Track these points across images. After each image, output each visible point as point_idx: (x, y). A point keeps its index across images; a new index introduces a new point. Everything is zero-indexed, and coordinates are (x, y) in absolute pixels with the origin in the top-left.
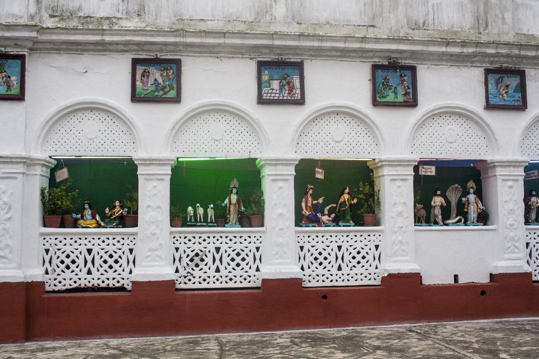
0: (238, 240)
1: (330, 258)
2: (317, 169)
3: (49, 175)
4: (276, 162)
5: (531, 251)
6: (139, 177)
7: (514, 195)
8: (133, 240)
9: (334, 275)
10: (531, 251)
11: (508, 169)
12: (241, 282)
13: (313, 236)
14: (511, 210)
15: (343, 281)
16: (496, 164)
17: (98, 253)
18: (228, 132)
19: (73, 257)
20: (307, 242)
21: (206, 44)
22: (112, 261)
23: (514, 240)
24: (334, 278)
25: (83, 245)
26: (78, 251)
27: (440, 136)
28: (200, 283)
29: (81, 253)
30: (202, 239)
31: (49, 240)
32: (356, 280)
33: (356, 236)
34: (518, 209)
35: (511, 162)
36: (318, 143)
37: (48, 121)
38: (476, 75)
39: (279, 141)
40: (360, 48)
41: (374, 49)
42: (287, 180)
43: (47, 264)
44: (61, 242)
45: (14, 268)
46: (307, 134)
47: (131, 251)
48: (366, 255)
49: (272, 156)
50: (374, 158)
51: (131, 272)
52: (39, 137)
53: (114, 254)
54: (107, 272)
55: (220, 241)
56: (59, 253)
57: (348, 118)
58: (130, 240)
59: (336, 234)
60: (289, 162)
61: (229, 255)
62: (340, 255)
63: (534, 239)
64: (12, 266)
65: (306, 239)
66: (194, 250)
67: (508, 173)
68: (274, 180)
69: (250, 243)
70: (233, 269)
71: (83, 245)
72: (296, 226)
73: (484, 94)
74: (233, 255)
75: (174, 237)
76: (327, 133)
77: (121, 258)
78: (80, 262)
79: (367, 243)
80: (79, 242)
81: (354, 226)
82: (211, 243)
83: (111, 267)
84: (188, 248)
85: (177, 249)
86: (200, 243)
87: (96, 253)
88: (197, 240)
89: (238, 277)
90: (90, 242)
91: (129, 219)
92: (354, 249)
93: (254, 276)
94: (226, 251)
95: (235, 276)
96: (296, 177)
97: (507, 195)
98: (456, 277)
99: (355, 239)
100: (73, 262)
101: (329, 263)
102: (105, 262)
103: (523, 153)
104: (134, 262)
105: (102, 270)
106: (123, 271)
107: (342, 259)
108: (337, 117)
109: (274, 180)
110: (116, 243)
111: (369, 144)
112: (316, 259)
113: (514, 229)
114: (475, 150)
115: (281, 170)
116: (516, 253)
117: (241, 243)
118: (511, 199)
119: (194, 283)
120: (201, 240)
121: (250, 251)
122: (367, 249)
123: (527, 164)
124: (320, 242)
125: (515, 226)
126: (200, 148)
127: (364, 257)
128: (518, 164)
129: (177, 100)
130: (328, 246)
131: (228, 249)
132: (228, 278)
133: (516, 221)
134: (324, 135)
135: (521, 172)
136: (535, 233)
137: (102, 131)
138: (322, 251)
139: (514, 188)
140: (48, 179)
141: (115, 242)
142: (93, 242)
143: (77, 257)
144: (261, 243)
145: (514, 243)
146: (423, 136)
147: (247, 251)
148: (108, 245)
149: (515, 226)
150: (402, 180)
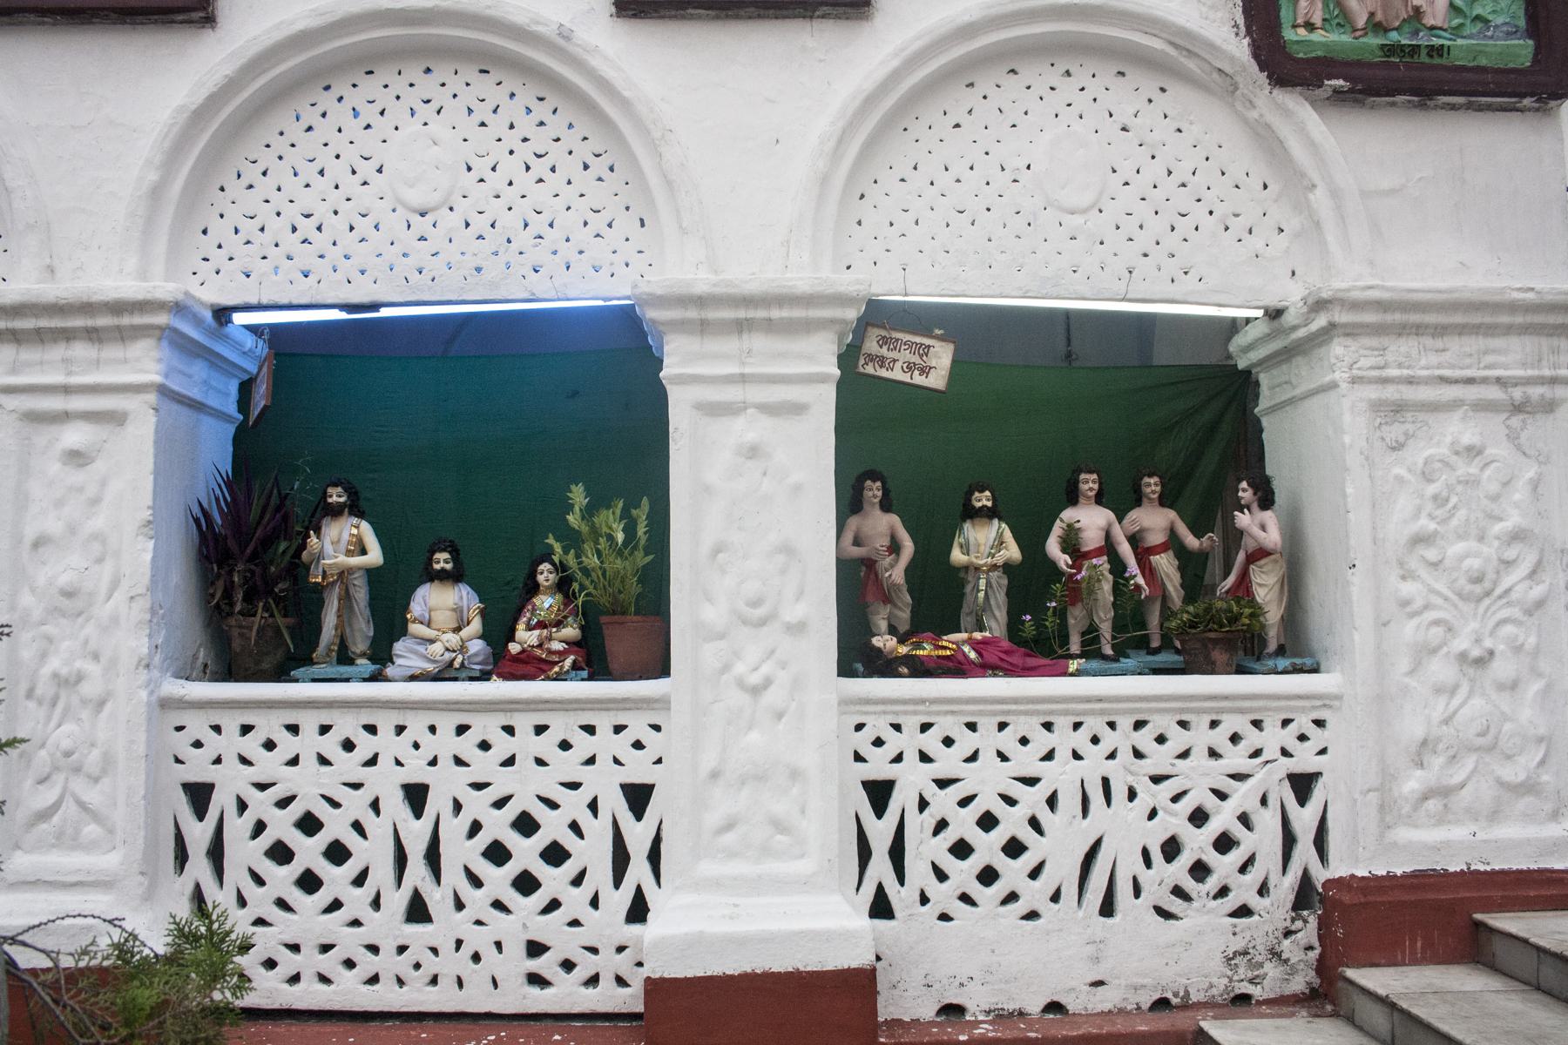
7: (95, 501)
8: (648, 737)
11: (57, 352)
12: (324, 979)
13: (486, 726)
14: (69, 594)
15: (434, 981)
18: (482, 166)
19: (553, 828)
20: (911, 757)
23: (77, 770)
29: (593, 806)
30: (472, 737)
31: (426, 739)
33: (509, 730)
34: (115, 585)
37: (871, 100)
42: (798, 409)
44: (1161, 739)
45: (804, 884)
47: (638, 796)
48: (1238, 831)
49: (702, 281)
50: (1273, 302)
51: (638, 911)
52: (156, 193)
55: (890, 750)
56: (942, 804)
59: (397, 718)
64: (804, 867)
65: (446, 743)
67: (57, 378)
72: (845, 670)
74: (498, 826)
77: (1040, 831)
82: (604, 761)
87: (231, 810)
91: (623, 630)
99: (503, 746)
100: (555, 855)
102: (280, 853)
106: (376, 904)
109: (36, 418)
112: (961, 850)
113: (84, 702)
115: (762, 354)
116: (91, 847)
118: (72, 530)
119: (295, 979)
120: (330, 745)
122: (1243, 796)
124: (988, 757)
125: (89, 689)
127: (1014, 848)
128: (103, 321)
130: (1031, 781)
133: (96, 657)
134: (351, 184)
139: (99, 466)
141: (330, 745)
142: (894, 742)
144: (1323, 752)
145: (78, 785)
149: (89, 689)
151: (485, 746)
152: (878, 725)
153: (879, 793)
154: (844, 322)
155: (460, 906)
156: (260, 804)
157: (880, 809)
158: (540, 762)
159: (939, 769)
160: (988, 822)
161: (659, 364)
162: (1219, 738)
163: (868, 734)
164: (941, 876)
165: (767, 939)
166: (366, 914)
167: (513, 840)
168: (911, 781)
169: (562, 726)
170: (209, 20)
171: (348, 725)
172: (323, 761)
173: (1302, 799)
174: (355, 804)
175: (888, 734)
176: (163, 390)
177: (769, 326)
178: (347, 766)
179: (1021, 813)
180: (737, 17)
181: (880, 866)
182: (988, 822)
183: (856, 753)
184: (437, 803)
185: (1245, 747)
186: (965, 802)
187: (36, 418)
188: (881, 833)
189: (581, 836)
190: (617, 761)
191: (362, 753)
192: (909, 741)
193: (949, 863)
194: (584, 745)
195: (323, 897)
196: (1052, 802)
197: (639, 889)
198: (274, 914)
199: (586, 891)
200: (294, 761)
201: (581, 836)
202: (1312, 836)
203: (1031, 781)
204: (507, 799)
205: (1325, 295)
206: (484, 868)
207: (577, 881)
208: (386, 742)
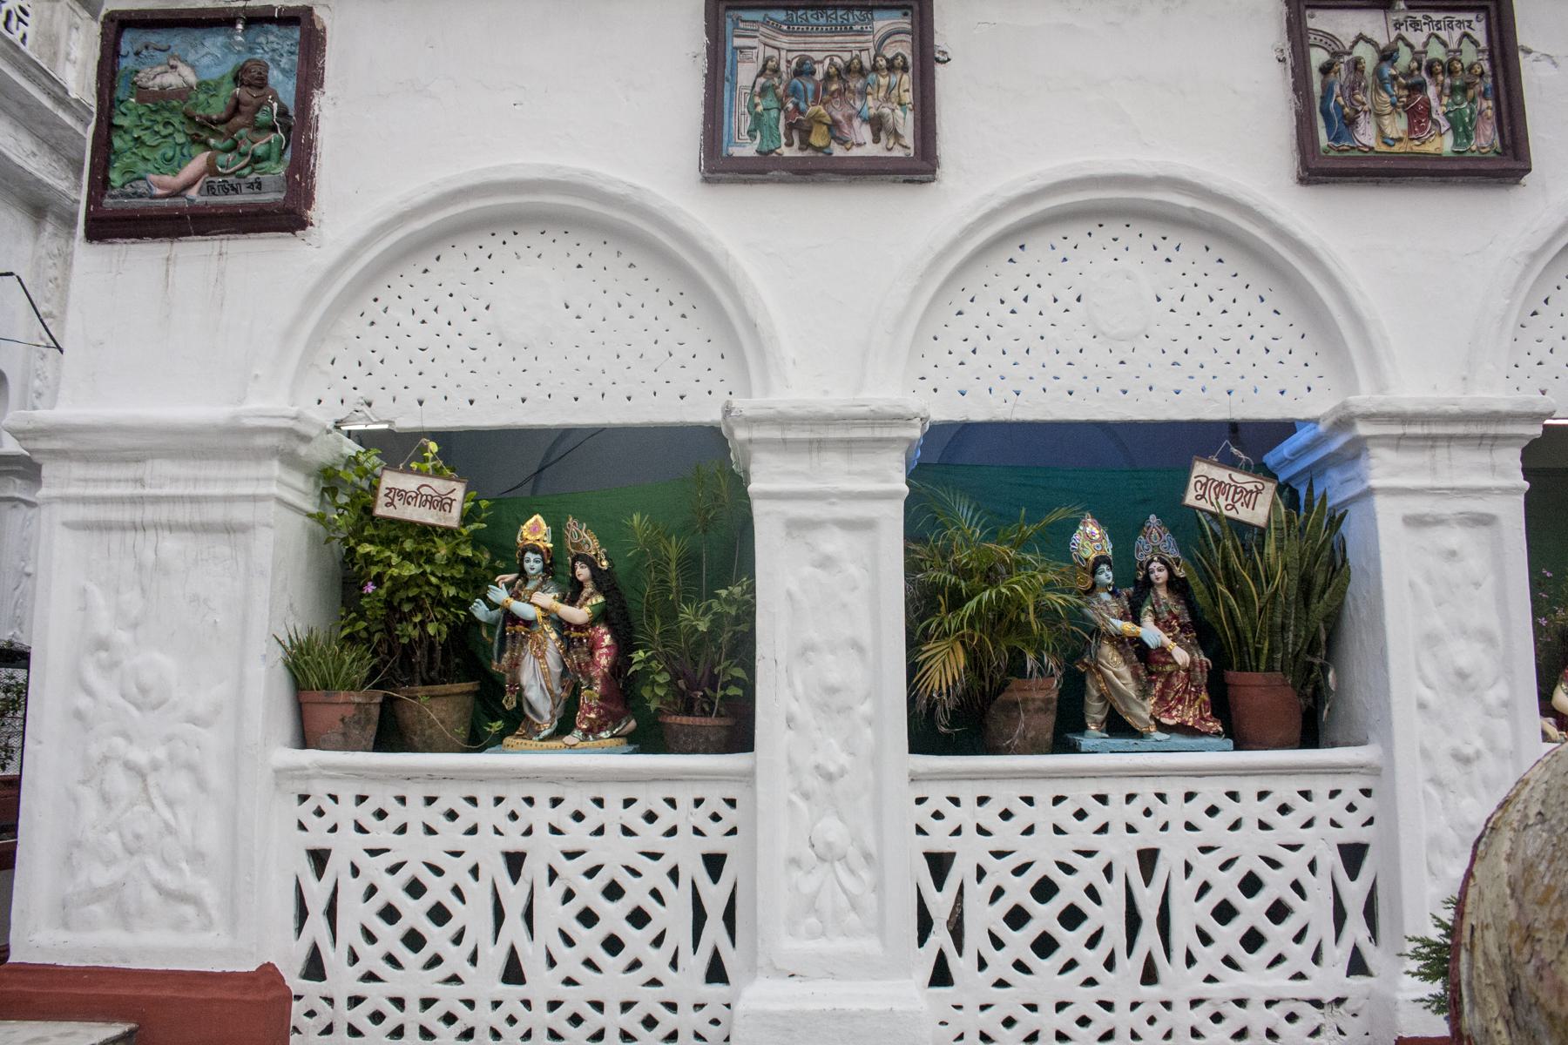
0: (1043, 814)
1: (1202, 912)
4: (820, 434)
6: (758, 508)
9: (483, 1006)
16: (1363, 429)
17: (1188, 868)
19: (439, 889)
20: (969, 830)
26: (1098, 863)
35: (829, 420)
39: (836, 345)
43: (317, 923)
46: (1178, 305)
47: (714, 864)
54: (597, 969)
58: (1341, 801)
61: (372, 891)
63: (981, 831)
66: (399, 866)
69: (1103, 829)
71: (1322, 825)
72: (911, 752)
73: (697, 113)
75: (304, 798)
76: (1068, 298)
78: (473, 915)
79: (464, 842)
80: (468, 815)
82: (685, 831)
83: (613, 945)
85: (319, 859)
86: (1263, 826)
90: (716, 817)
92: (1225, 866)
93: (699, 1006)
96: (1528, 495)
97: (1435, 592)
107: (528, 916)
109: (1416, 522)
110: (637, 823)
115: (839, 473)
120: (634, 817)
129: (920, 166)
130: (1089, 854)
132: (564, 1012)
136: (1189, 796)
137: (1171, 298)
142: (954, 816)
150: (848, 525)
151: (578, 816)
152: (938, 801)
153: (939, 865)
154: (911, 441)
155: (552, 963)
156: (999, 872)
158: (1058, 830)
160: (613, 892)
163: (928, 808)
164: (998, 944)
166: (665, 973)
168: (969, 853)
169: (1211, 791)
171: (577, 798)
172: (430, 831)
173: (1353, 874)
174: (1295, 865)
175: (391, 806)
177: (849, 446)
178: (452, 835)
181: (940, 937)
182: (613, 892)
183: (1260, 822)
185: (463, 823)
186: (591, 873)
189: (463, 900)
190: (497, 832)
191: (1093, 822)
192: (968, 815)
193: (1212, 927)
194: (1097, 814)
195: (1058, 958)
198: (1013, 975)
201: (463, 900)
202: (1156, 912)
204: (598, 868)
207: (658, 942)
208: (1117, 812)
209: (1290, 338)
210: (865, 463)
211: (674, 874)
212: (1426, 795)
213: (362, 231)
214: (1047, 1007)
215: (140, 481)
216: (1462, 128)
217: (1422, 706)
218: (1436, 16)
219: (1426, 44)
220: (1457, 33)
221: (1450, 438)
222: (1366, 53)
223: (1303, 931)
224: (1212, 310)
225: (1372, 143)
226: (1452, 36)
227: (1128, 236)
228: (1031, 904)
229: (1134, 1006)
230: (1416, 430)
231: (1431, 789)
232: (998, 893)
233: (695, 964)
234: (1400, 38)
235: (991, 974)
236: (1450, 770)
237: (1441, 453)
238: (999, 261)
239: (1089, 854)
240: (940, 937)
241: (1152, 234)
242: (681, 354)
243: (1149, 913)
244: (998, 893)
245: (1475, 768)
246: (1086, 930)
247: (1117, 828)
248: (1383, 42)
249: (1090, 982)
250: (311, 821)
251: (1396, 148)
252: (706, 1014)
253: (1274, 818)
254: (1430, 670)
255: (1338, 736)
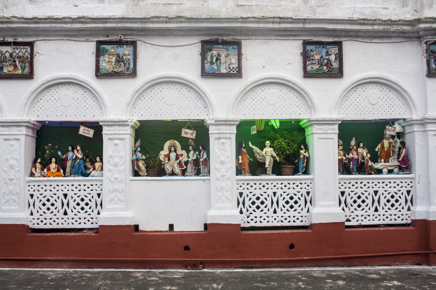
2: (387, 127)
3: (35, 136)
4: (219, 123)
5: (305, 198)
10: (305, 198)
19: (296, 198)
21: (149, 29)
22: (83, 203)
24: (60, 221)
25: (371, 188)
27: (389, 99)
28: (294, 221)
29: (92, 197)
32: (379, 220)
36: (291, 106)
38: (88, 48)
39: (223, 105)
40: (384, 29)
41: (345, 29)
52: (26, 104)
53: (85, 198)
56: (386, 194)
57: (75, 86)
58: (407, 184)
60: (18, 124)
62: (65, 202)
68: (216, 139)
69: (402, 187)
70: (389, 209)
71: (371, 188)
75: (29, 186)
76: (57, 99)
77: (300, 200)
81: (147, 176)
83: (83, 209)
84: (41, 195)
86: (395, 187)
88: (258, 186)
89: (258, 218)
90: (88, 188)
92: (355, 194)
94: (383, 194)
95: (46, 219)
98: (171, 227)
101: (299, 206)
103: (33, 114)
104: (311, 202)
105: (386, 208)
107: (34, 205)
108: (270, 85)
109: (6, 140)
111: (399, 106)
114: (378, 111)
115: (224, 129)
117: (361, 188)
120: (261, 186)
121: (369, 194)
123: (340, 122)
126: (387, 111)
130: (265, 193)
131: (74, 196)
135: (234, 130)
138: (50, 198)
140: (337, 135)
141: (295, 186)
143: (90, 200)
144: (101, 190)
146: (49, 101)
147: (366, 194)
148: (357, 188)
150: (120, 139)
157: (241, 196)
159: (385, 189)
161: (208, 130)
162: (350, 185)
163: (239, 185)
164: (284, 207)
165: (15, 219)
167: (46, 202)
168: (347, 191)
170: (33, 78)
173: (376, 195)
174: (265, 195)
176: (26, 135)
177: (119, 125)
179: (264, 197)
180: (232, 78)
184: (69, 197)
187: (6, 140)
188: (241, 200)
191: (90, 189)
193: (285, 205)
194: (300, 186)
196: (402, 194)
197: (275, 209)
198: (78, 213)
199: (301, 208)
200: (46, 191)
203: (366, 191)
205: (311, 119)
206: (76, 206)
208: (371, 185)
209: (401, 104)
210: (331, 127)
211: (302, 195)
212: (4, 185)
213: (38, 86)
214: (292, 217)
215: (219, 130)
216: (23, 69)
217: (4, 171)
218: (21, 47)
219: (19, 53)
220: (25, 50)
221: (12, 125)
222: (7, 55)
223: (300, 205)
224: (388, 100)
225: (6, 72)
226: (24, 51)
227: (172, 87)
228: (357, 199)
229: (373, 215)
230: (5, 124)
231: (5, 184)
232: (250, 199)
233: (272, 210)
234: (14, 51)
235: (39, 214)
236: (8, 182)
237: (11, 128)
238: (46, 92)
239: (55, 194)
240: (241, 205)
241: (379, 86)
242: (198, 107)
243: (99, 204)
244: (250, 199)
245: (13, 181)
246: (265, 205)
247: (404, 187)
248: (11, 52)
249: (400, 211)
250: (239, 188)
251: (11, 73)
252: (407, 216)
253: (295, 187)
254: (6, 165)
255: (283, 173)
